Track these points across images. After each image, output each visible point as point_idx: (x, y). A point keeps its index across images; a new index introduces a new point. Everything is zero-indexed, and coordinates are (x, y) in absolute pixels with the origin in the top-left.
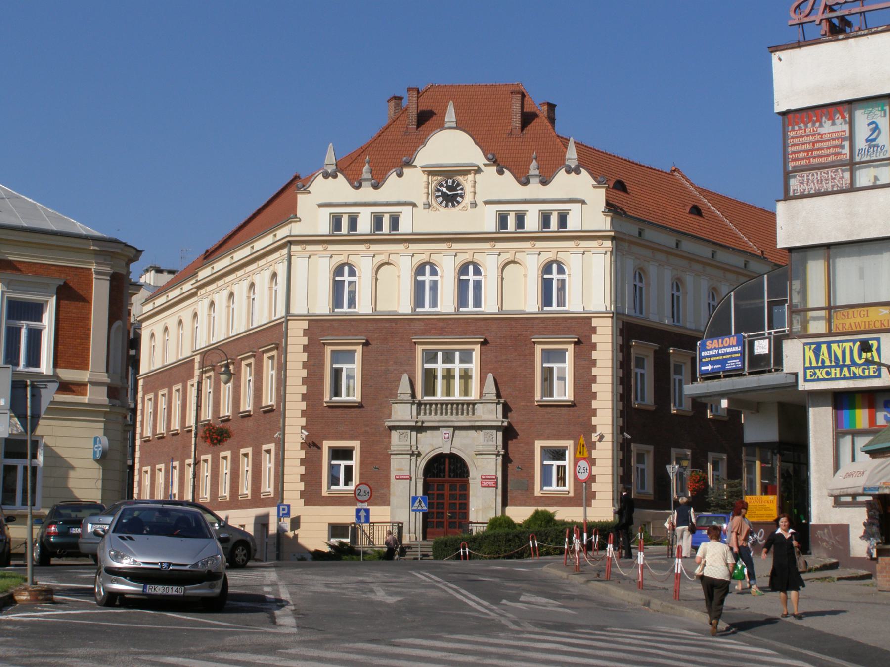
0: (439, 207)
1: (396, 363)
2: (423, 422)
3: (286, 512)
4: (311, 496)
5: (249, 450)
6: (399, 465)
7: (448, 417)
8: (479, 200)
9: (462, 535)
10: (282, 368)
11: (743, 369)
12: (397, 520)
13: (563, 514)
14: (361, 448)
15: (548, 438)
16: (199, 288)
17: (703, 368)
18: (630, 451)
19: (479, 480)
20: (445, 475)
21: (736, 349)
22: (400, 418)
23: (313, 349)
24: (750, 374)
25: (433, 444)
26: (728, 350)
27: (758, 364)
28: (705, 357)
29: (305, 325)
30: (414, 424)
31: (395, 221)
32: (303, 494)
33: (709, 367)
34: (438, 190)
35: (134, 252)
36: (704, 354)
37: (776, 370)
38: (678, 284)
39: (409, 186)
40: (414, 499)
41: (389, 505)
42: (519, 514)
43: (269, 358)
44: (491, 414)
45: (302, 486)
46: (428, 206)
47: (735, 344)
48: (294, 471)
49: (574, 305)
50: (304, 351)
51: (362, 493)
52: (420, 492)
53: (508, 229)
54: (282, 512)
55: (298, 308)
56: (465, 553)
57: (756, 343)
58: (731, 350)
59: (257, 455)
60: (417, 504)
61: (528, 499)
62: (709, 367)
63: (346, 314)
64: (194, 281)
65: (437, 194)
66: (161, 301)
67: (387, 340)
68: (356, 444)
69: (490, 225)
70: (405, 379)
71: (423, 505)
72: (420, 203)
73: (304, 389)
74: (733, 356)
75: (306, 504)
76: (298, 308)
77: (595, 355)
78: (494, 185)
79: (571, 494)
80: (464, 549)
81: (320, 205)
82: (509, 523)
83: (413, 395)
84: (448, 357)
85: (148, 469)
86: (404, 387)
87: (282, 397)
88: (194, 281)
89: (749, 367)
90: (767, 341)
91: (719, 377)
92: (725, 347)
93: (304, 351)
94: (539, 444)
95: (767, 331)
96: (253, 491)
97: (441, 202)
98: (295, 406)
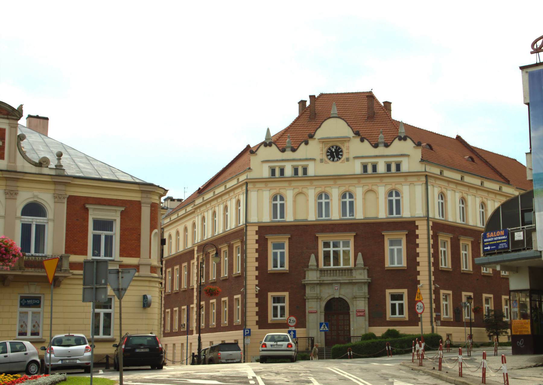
2: (323, 281)
5: (226, 299)
6: (311, 305)
7: (335, 278)
9: (348, 345)
10: (244, 252)
11: (508, 248)
12: (310, 336)
13: (402, 330)
16: (196, 209)
17: (485, 248)
18: (439, 294)
19: (355, 312)
21: (504, 237)
22: (310, 279)
23: (262, 243)
24: (513, 251)
25: (328, 293)
26: (500, 238)
27: (518, 246)
28: (486, 242)
29: (257, 228)
30: (318, 282)
32: (257, 323)
33: (489, 248)
35: (164, 191)
36: (485, 240)
37: (528, 249)
38: (463, 201)
39: (313, 150)
40: (321, 324)
41: (305, 327)
42: (379, 331)
44: (362, 276)
45: (257, 318)
46: (322, 161)
47: (503, 234)
48: (252, 309)
49: (406, 214)
51: (291, 321)
52: (323, 321)
53: (369, 171)
54: (246, 333)
55: (253, 219)
56: (350, 354)
57: (516, 234)
58: (501, 238)
59: (231, 300)
60: (322, 327)
61: (383, 322)
62: (489, 248)
63: (279, 221)
64: (193, 206)
66: (174, 217)
67: (303, 236)
68: (286, 294)
69: (358, 169)
70: (313, 256)
71: (326, 327)
73: (257, 264)
74: (503, 241)
75: (259, 328)
76: (253, 219)
77: (418, 241)
78: (358, 148)
79: (407, 319)
80: (350, 352)
82: (372, 336)
83: (318, 266)
84: (335, 245)
85: (169, 310)
87: (244, 269)
88: (193, 206)
89: (512, 247)
90: (522, 233)
91: (494, 254)
92: (497, 237)
95: (521, 227)
96: (229, 321)
97: (330, 159)
98: (252, 273)
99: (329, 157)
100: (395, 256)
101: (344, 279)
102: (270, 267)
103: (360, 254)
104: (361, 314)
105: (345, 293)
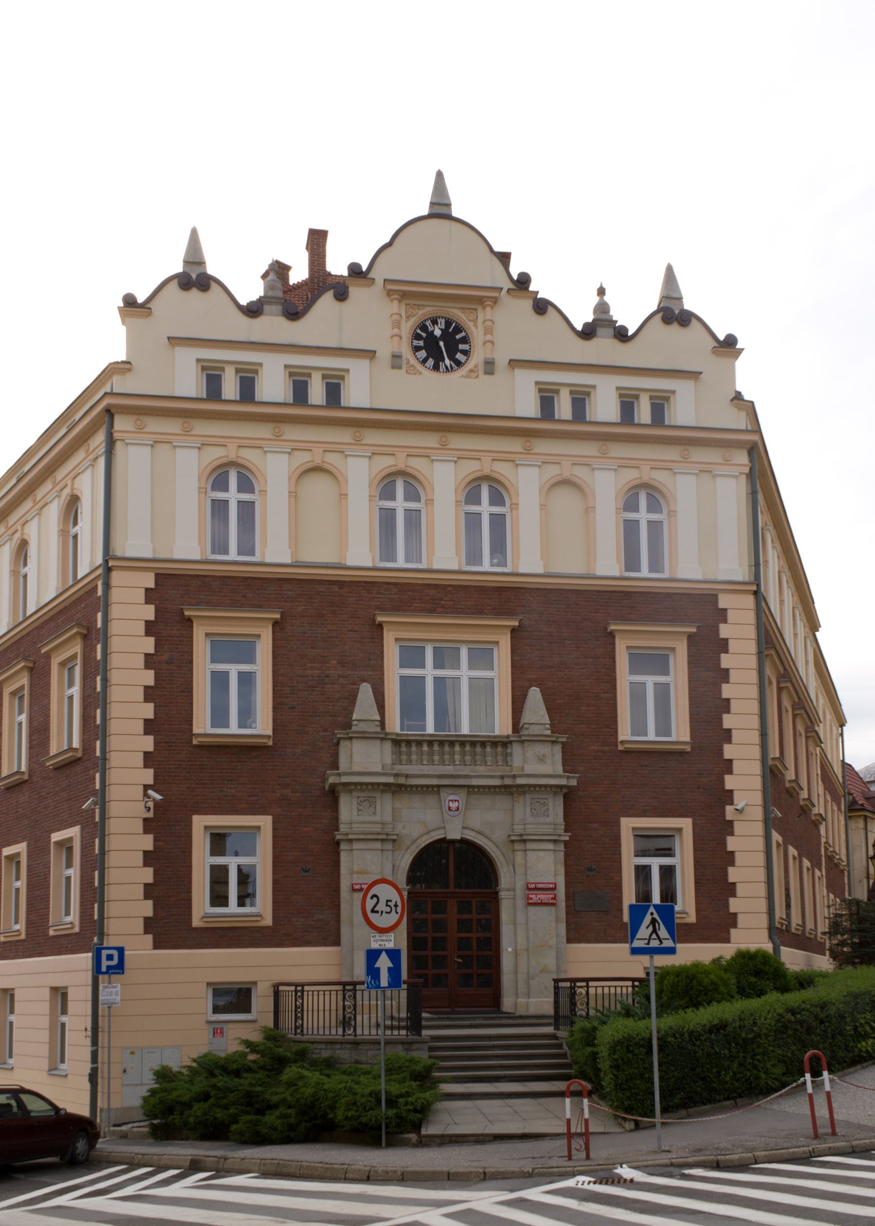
0: (419, 367)
1: (342, 663)
3: (115, 962)
4: (170, 925)
6: (358, 865)
8: (502, 361)
14: (274, 829)
15: (644, 814)
19: (520, 892)
20: (454, 887)
25: (423, 823)
29: (149, 581)
31: (334, 392)
32: (149, 925)
34: (424, 327)
43: (62, 664)
44: (542, 763)
46: (396, 360)
50: (148, 633)
51: (381, 907)
54: (105, 963)
55: (134, 543)
59: (39, 852)
65: (416, 343)
69: (527, 405)
70: (366, 691)
72: (384, 353)
75: (156, 946)
81: (174, 341)
86: (364, 706)
87: (95, 730)
93: (148, 633)
94: (628, 825)
99: (423, 354)
100: (650, 706)
101: (484, 773)
102: (203, 724)
103: (535, 695)
104: (545, 897)
105: (479, 822)
